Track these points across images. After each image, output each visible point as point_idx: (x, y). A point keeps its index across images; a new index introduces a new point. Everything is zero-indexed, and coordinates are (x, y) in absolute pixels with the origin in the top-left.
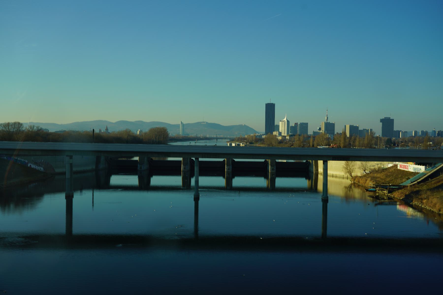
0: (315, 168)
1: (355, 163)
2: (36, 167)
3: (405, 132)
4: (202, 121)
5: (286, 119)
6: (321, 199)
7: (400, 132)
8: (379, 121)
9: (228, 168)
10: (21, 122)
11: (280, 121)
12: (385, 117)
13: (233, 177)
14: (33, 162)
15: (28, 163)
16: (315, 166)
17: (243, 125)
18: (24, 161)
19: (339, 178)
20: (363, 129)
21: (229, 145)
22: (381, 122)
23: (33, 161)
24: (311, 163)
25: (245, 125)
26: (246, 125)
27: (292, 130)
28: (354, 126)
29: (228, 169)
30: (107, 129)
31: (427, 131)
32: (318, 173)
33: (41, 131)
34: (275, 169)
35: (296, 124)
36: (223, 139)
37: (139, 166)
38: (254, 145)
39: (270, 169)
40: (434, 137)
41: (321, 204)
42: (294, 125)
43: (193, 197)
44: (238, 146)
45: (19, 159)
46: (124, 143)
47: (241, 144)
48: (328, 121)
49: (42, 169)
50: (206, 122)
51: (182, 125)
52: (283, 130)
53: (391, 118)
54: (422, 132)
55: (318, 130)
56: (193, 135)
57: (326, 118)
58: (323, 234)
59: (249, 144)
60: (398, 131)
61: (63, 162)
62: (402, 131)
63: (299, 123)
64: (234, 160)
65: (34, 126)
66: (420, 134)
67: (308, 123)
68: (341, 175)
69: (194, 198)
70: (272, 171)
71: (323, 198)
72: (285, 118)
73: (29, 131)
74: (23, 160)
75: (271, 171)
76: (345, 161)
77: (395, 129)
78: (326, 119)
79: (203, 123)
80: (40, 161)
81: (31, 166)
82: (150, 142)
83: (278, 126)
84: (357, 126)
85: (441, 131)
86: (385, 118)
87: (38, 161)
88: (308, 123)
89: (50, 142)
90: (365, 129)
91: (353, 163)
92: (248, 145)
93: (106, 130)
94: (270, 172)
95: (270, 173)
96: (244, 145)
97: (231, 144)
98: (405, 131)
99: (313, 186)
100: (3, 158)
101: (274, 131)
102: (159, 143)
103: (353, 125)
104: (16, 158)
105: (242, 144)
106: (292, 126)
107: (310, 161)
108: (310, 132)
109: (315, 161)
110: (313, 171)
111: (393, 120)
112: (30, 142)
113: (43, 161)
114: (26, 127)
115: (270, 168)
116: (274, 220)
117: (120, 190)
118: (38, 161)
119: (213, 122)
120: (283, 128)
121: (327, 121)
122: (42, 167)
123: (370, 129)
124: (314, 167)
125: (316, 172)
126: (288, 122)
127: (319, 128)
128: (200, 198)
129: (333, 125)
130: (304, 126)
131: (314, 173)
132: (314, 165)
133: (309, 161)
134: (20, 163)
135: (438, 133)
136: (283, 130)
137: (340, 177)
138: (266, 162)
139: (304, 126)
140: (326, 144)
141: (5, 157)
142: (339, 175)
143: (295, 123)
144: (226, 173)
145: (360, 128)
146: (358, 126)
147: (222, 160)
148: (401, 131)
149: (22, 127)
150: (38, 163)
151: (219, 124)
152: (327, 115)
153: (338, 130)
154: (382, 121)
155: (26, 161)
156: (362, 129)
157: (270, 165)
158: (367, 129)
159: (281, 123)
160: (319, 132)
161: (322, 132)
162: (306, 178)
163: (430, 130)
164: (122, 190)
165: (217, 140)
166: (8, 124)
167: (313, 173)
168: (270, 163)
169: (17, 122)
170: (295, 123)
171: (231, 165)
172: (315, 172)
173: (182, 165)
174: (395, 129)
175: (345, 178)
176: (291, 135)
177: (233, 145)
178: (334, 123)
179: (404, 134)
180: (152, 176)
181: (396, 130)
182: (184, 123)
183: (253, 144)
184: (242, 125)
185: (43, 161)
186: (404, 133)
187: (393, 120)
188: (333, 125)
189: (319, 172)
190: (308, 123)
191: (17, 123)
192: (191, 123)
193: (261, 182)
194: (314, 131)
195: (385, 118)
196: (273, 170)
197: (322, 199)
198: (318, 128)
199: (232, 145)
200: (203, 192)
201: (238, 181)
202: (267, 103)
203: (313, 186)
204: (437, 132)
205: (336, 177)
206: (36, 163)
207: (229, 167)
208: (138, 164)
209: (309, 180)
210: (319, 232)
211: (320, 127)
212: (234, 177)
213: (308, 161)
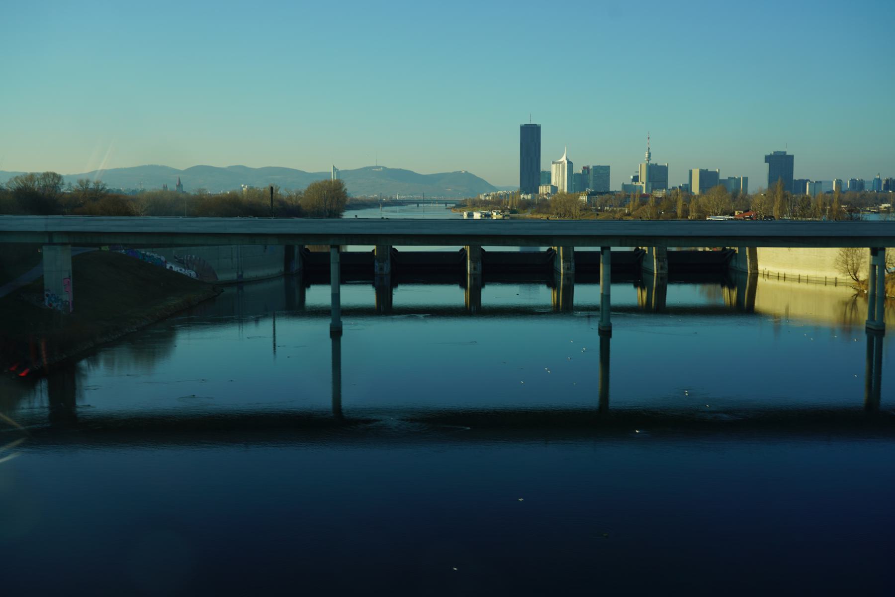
0: (750, 263)
1: (863, 251)
2: (181, 270)
3: (816, 182)
4: (374, 165)
5: (567, 159)
6: (597, 331)
7: (807, 183)
8: (763, 160)
9: (566, 267)
10: (58, 172)
11: (553, 163)
12: (776, 151)
13: (395, 285)
14: (176, 260)
15: (166, 262)
16: (751, 260)
17: (463, 172)
18: (159, 257)
19: (816, 283)
20: (729, 178)
21: (465, 216)
22: (766, 162)
23: (176, 258)
24: (647, 252)
25: (466, 172)
26: (469, 172)
27: (578, 180)
28: (709, 170)
29: (568, 268)
30: (180, 185)
31: (862, 180)
32: (758, 273)
33: (103, 192)
34: (666, 266)
35: (586, 169)
36: (431, 203)
37: (376, 264)
38: (521, 215)
39: (657, 267)
40: (878, 191)
41: (597, 338)
42: (581, 172)
43: (597, 328)
44: (486, 218)
45: (148, 254)
46: (266, 216)
47: (495, 214)
48: (652, 162)
49: (193, 274)
50: (383, 167)
51: (335, 173)
52: (559, 182)
53: (787, 154)
54: (853, 181)
55: (631, 181)
56: (374, 196)
57: (647, 155)
58: (601, 407)
59: (508, 213)
60: (803, 180)
61: (232, 259)
62: (811, 181)
63: (591, 167)
64: (395, 249)
65: (88, 181)
66: (848, 187)
67: (611, 167)
68: (819, 278)
69: (332, 332)
70: (659, 271)
71: (601, 329)
72: (563, 156)
73: (79, 191)
74: (156, 256)
75: (657, 270)
76: (843, 249)
77: (796, 177)
78: (647, 157)
79: (377, 170)
80: (188, 258)
81: (171, 267)
82: (318, 213)
83: (549, 174)
84: (716, 172)
85: (891, 179)
86: (774, 152)
87: (185, 258)
88: (609, 166)
89: (307, 217)
90: (732, 178)
91: (858, 251)
92: (508, 216)
93: (177, 186)
94: (657, 274)
95: (655, 275)
96: (500, 217)
97: (470, 215)
98: (818, 180)
99: (561, 303)
100: (119, 252)
101: (540, 185)
102: (318, 213)
103: (707, 170)
104: (144, 253)
105: (497, 214)
106: (577, 172)
107: (644, 248)
108: (615, 185)
109: (563, 249)
110: (747, 270)
111: (792, 157)
112: (250, 217)
113: (194, 256)
114: (70, 184)
115: (657, 265)
116: (856, 376)
117: (421, 316)
118: (185, 258)
119: (160, 164)
120: (559, 179)
121: (648, 161)
122: (193, 270)
123: (743, 178)
124: (748, 261)
125: (752, 272)
126: (570, 163)
127: (634, 177)
128: (613, 332)
129: (663, 170)
130: (602, 173)
131: (749, 274)
132: (748, 257)
133: (642, 249)
134: (150, 262)
135: (885, 183)
136: (559, 182)
137: (817, 282)
138: (639, 256)
139: (602, 173)
140: (722, 212)
141: (123, 251)
142: (816, 277)
143: (584, 168)
144: (563, 276)
145: (723, 176)
146: (717, 170)
147: (456, 249)
148: (809, 180)
149: (61, 183)
150: (185, 261)
151: (412, 170)
152: (649, 149)
153: (675, 180)
154: (768, 159)
155: (163, 259)
156: (727, 178)
157: (656, 258)
158: (737, 177)
159: (554, 166)
160: (635, 186)
161: (641, 186)
162: (636, 286)
163: (868, 175)
164: (427, 316)
165: (418, 206)
166: (31, 177)
167: (748, 273)
168: (656, 254)
169: (51, 173)
170: (584, 168)
171: (574, 260)
172: (751, 271)
173: (469, 261)
174: (796, 177)
175: (831, 283)
176: (591, 192)
177: (477, 216)
178: (666, 165)
179: (815, 188)
180: (309, 287)
181: (797, 179)
182: (339, 170)
183: (519, 213)
184: (461, 171)
185: (194, 256)
186: (815, 184)
187: (792, 157)
188: (663, 170)
189: (759, 272)
190: (609, 166)
191: (50, 175)
192: (349, 169)
193: (543, 295)
194: (623, 183)
195: (774, 152)
196: (662, 268)
197: (599, 329)
198: (632, 177)
199: (473, 216)
200: (543, 316)
201: (404, 295)
202: (523, 123)
203: (561, 303)
204: (884, 182)
205: (808, 281)
206: (180, 262)
207: (569, 264)
208: (376, 261)
209: (554, 289)
210: (590, 399)
211: (636, 174)
212: (396, 286)
213: (640, 248)
